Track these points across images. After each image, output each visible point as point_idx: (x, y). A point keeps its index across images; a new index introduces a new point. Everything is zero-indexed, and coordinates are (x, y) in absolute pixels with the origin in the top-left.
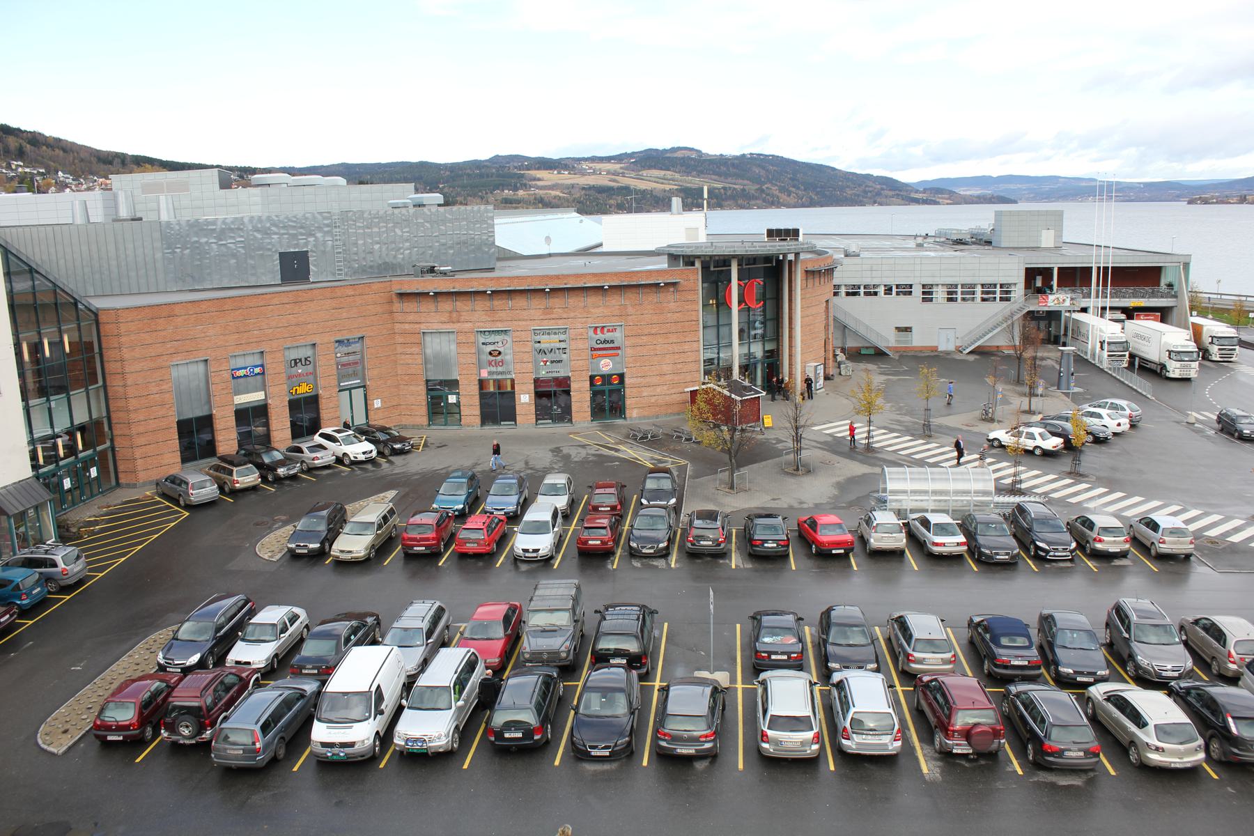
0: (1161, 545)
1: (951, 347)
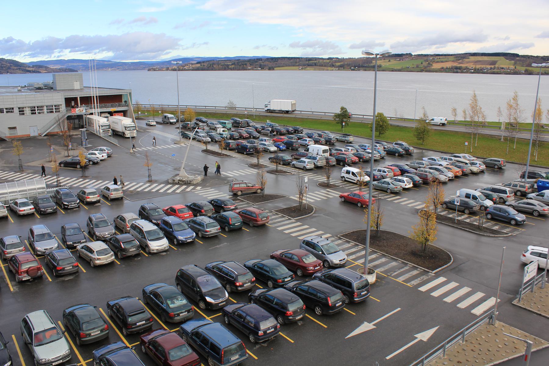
0: (111, 196)
1: (36, 134)
